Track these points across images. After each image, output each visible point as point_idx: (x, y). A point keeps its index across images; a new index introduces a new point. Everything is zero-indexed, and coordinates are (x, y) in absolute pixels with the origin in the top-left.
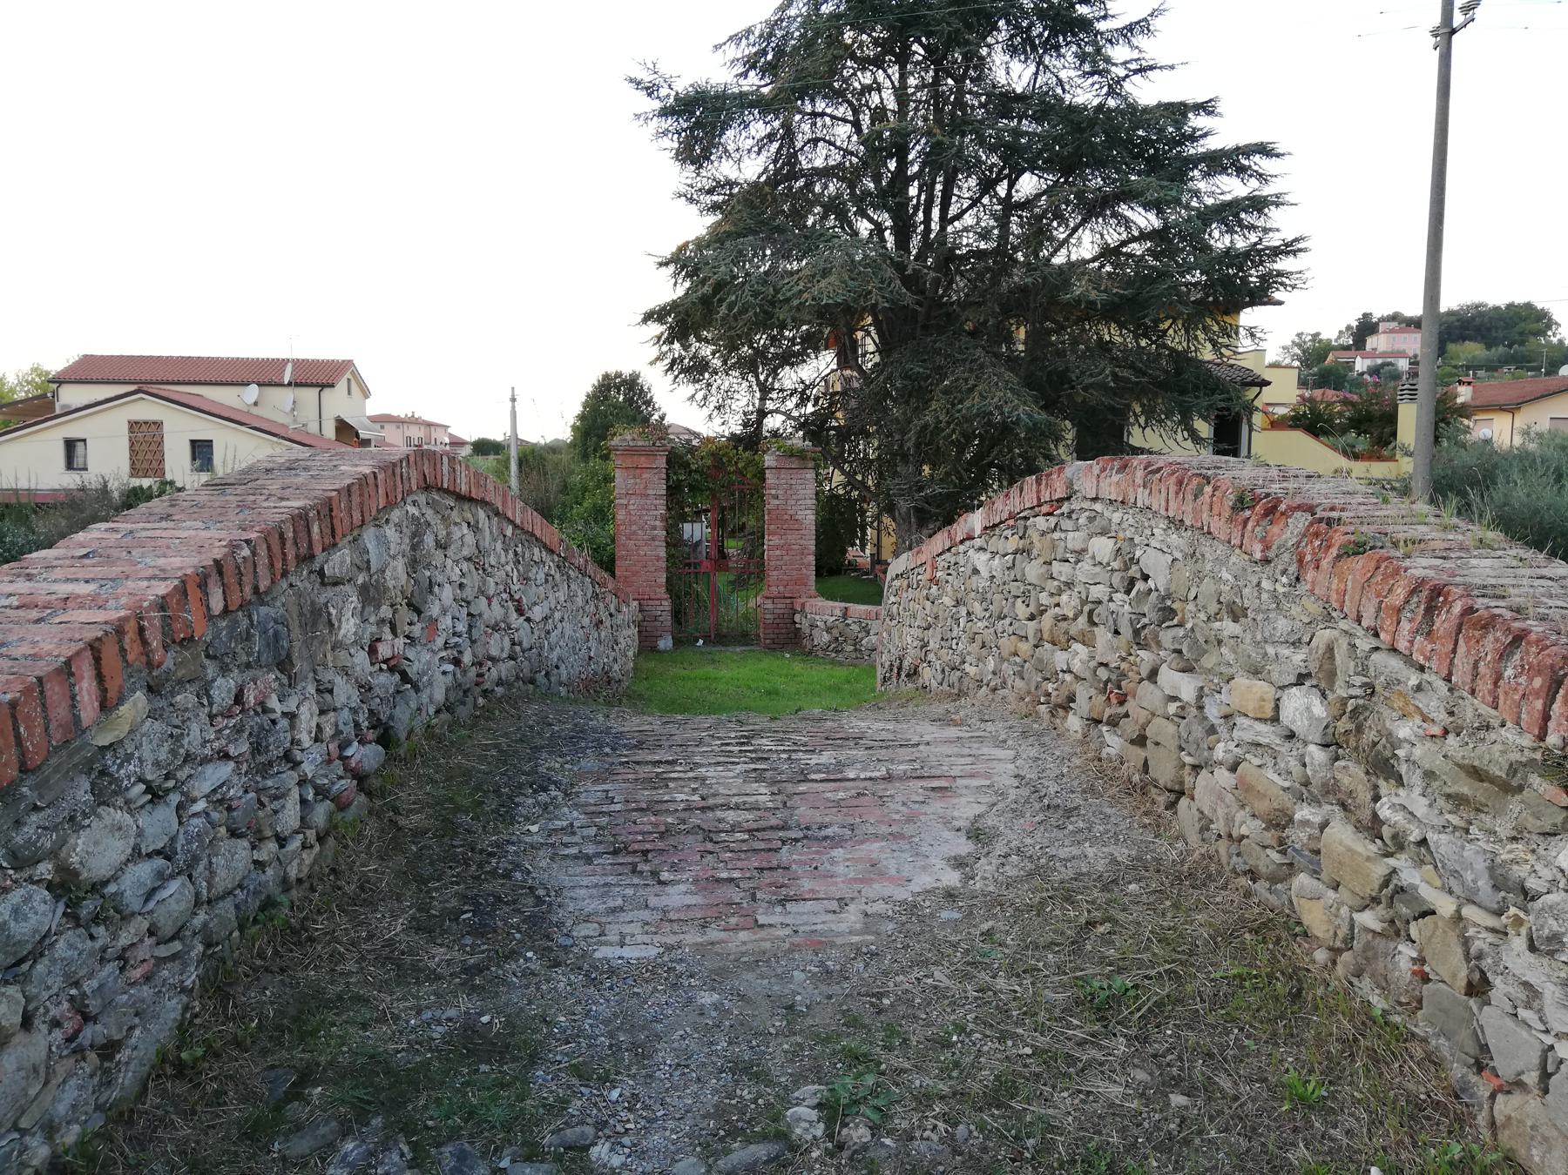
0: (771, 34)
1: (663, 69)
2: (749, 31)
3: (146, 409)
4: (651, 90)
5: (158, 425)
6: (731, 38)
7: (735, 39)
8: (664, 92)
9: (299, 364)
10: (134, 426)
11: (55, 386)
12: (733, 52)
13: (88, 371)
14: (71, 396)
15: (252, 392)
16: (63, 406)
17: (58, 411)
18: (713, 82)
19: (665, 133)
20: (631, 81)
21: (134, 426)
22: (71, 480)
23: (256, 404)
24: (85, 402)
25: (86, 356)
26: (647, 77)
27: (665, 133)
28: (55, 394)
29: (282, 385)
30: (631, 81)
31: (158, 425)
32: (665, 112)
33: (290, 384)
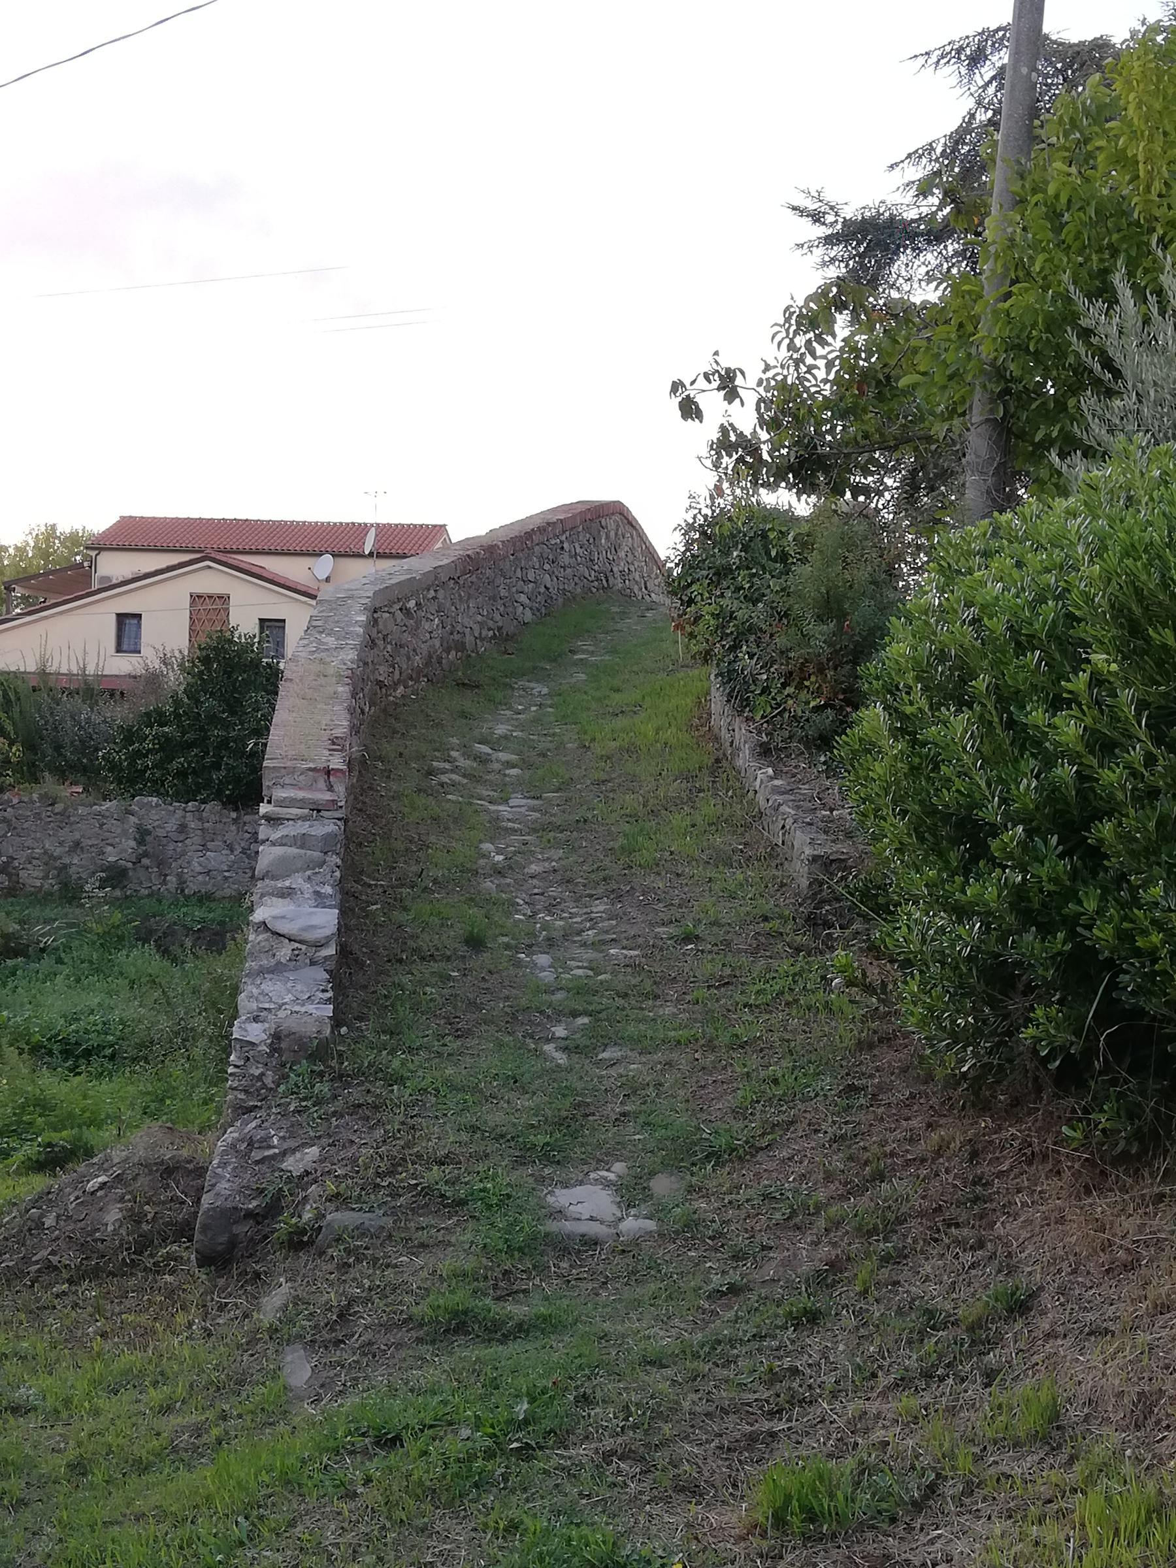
0: (955, 150)
1: (828, 196)
2: (930, 148)
3: (211, 581)
4: (817, 217)
5: (224, 599)
6: (909, 156)
7: (914, 156)
8: (830, 218)
9: (385, 531)
10: (196, 598)
11: (93, 553)
12: (916, 172)
13: (132, 535)
14: (113, 566)
15: (325, 565)
16: (105, 579)
17: (96, 586)
18: (759, 352)
19: (833, 260)
20: (794, 208)
21: (196, 598)
22: (123, 665)
23: (328, 580)
24: (164, 566)
25: (123, 518)
26: (812, 206)
27: (833, 260)
28: (93, 563)
29: (361, 556)
30: (794, 208)
31: (224, 599)
32: (829, 240)
33: (371, 554)
